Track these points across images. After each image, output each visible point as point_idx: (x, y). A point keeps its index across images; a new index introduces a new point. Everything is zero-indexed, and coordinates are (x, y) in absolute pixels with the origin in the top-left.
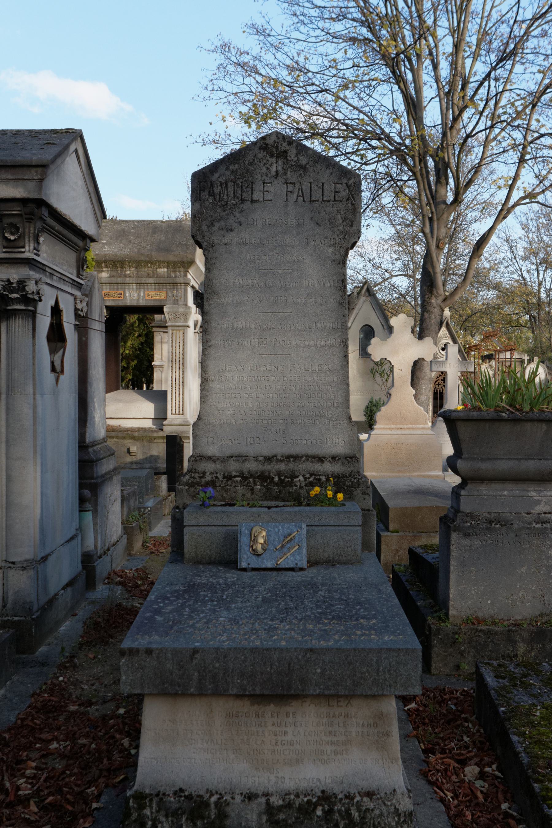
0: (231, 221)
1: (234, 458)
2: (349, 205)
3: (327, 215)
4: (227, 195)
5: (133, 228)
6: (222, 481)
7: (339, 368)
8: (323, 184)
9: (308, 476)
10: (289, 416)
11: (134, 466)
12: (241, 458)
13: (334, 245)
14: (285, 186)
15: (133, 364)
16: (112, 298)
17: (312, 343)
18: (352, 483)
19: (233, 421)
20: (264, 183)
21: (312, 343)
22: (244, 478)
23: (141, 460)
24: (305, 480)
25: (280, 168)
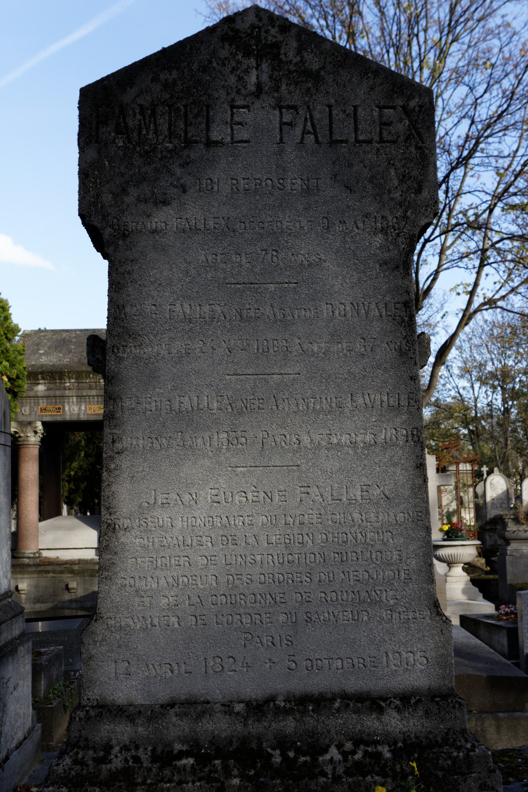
0: (163, 183)
1: (177, 709)
2: (413, 149)
3: (366, 171)
4: (156, 132)
5: (75, 338)
6: (149, 770)
7: (407, 493)
8: (355, 108)
9: (349, 746)
10: (301, 603)
11: (74, 605)
12: (193, 707)
13: (383, 231)
14: (277, 112)
15: (83, 486)
16: (50, 413)
17: (345, 439)
18: (455, 760)
19: (174, 620)
20: (232, 107)
21: (345, 439)
22: (203, 760)
23: (81, 597)
24: (345, 759)
25: (265, 78)
